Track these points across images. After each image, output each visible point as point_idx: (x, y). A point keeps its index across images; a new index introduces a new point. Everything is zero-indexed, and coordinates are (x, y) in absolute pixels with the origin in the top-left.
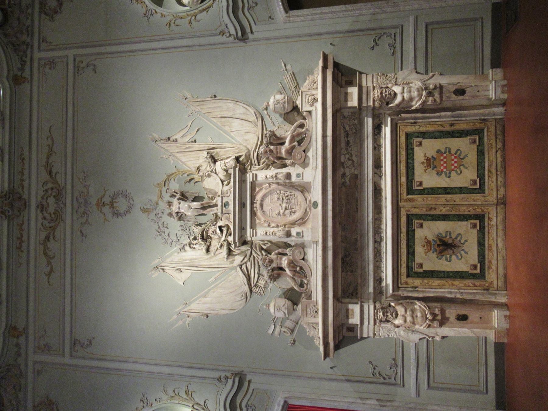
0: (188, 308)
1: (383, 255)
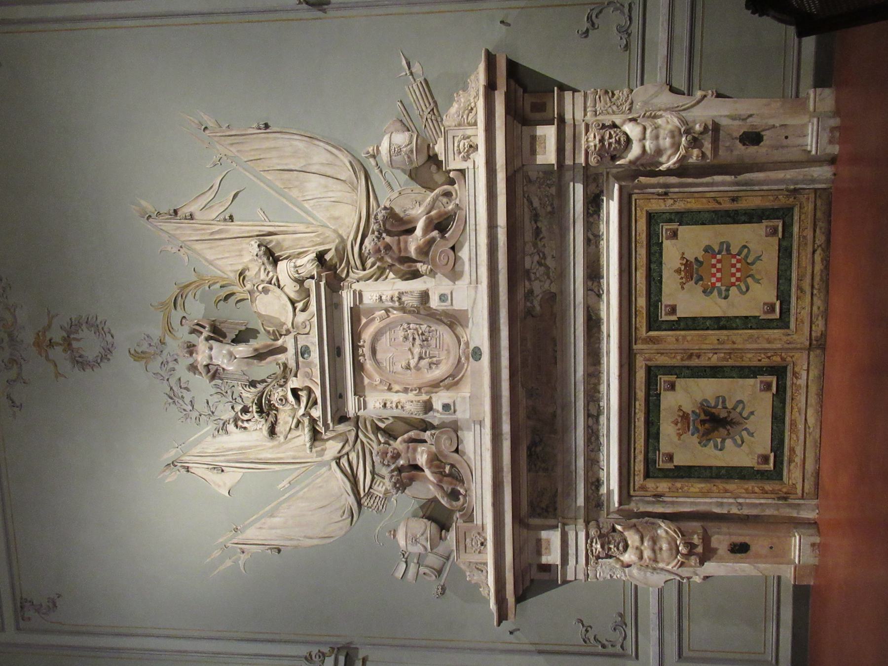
0: (240, 537)
1: (603, 440)
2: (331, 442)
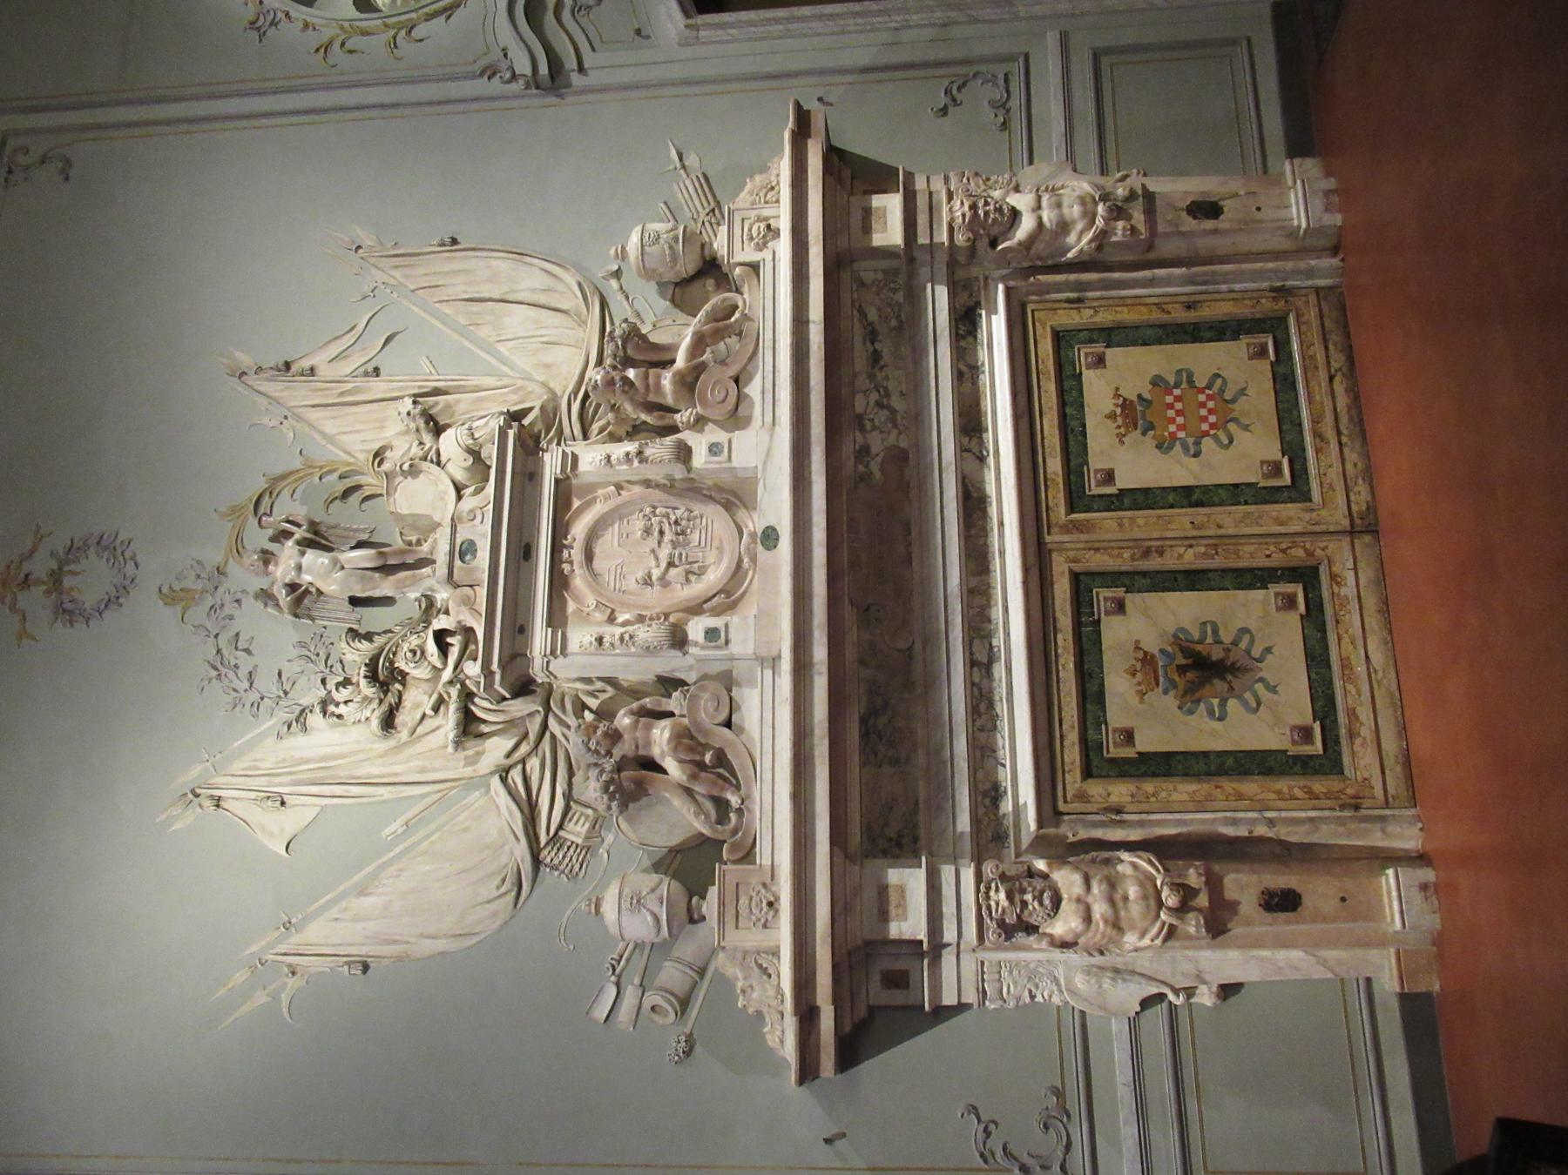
0: (293, 940)
1: (1002, 708)
2: (495, 738)
